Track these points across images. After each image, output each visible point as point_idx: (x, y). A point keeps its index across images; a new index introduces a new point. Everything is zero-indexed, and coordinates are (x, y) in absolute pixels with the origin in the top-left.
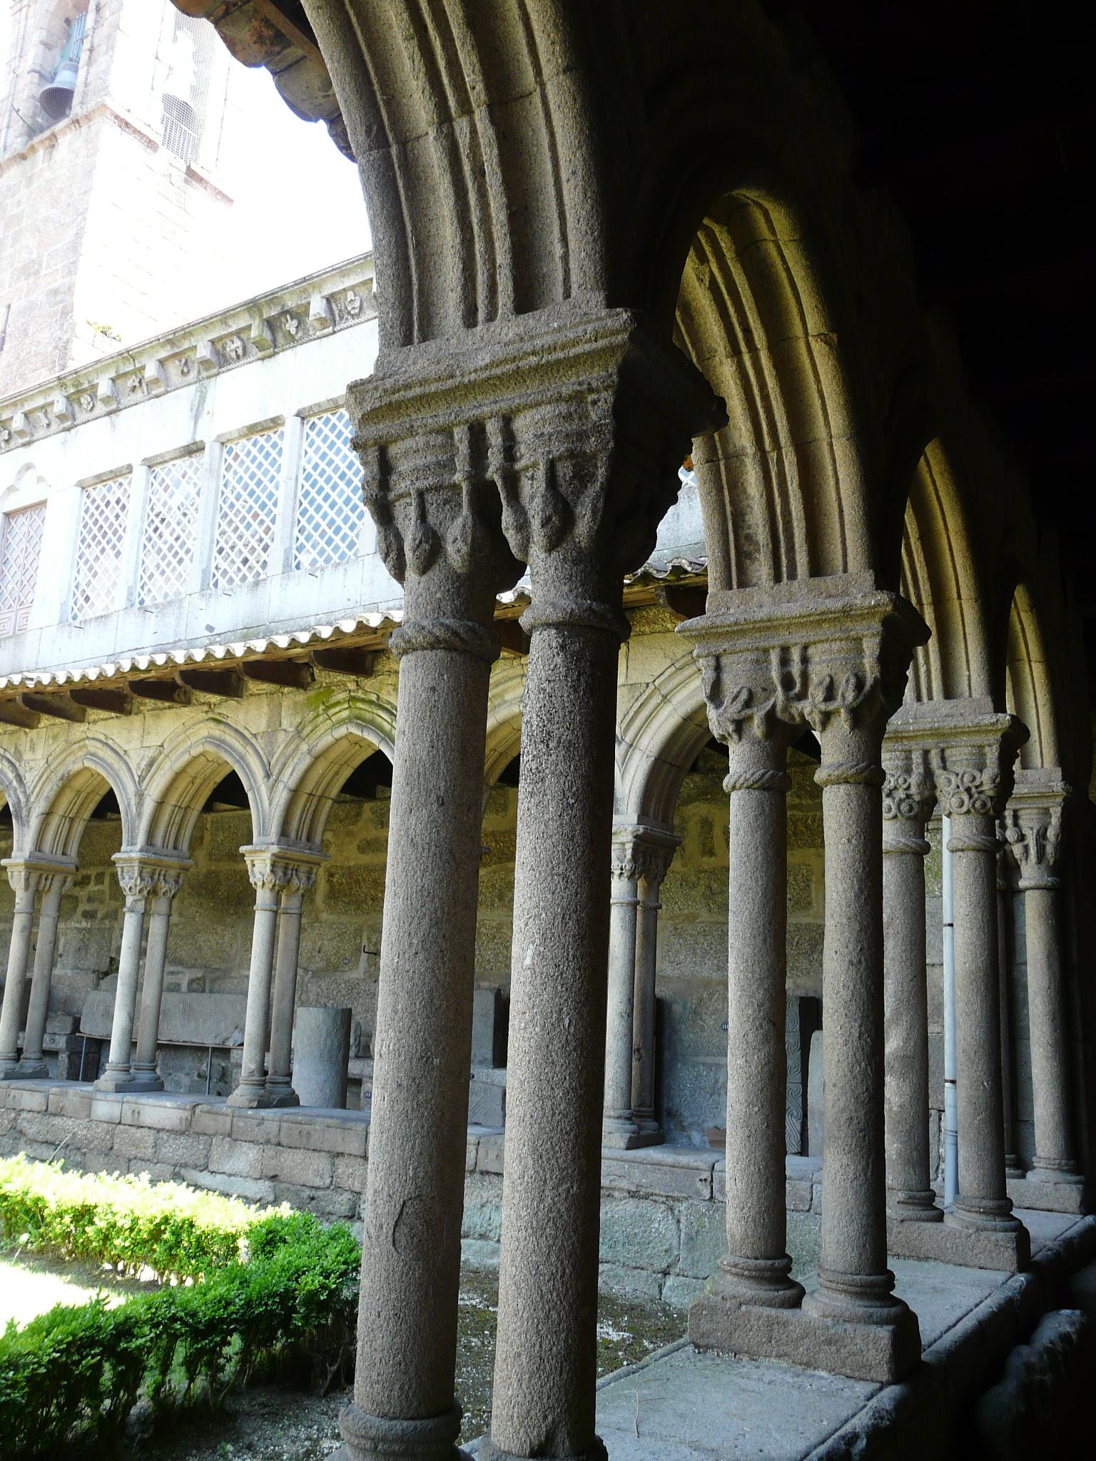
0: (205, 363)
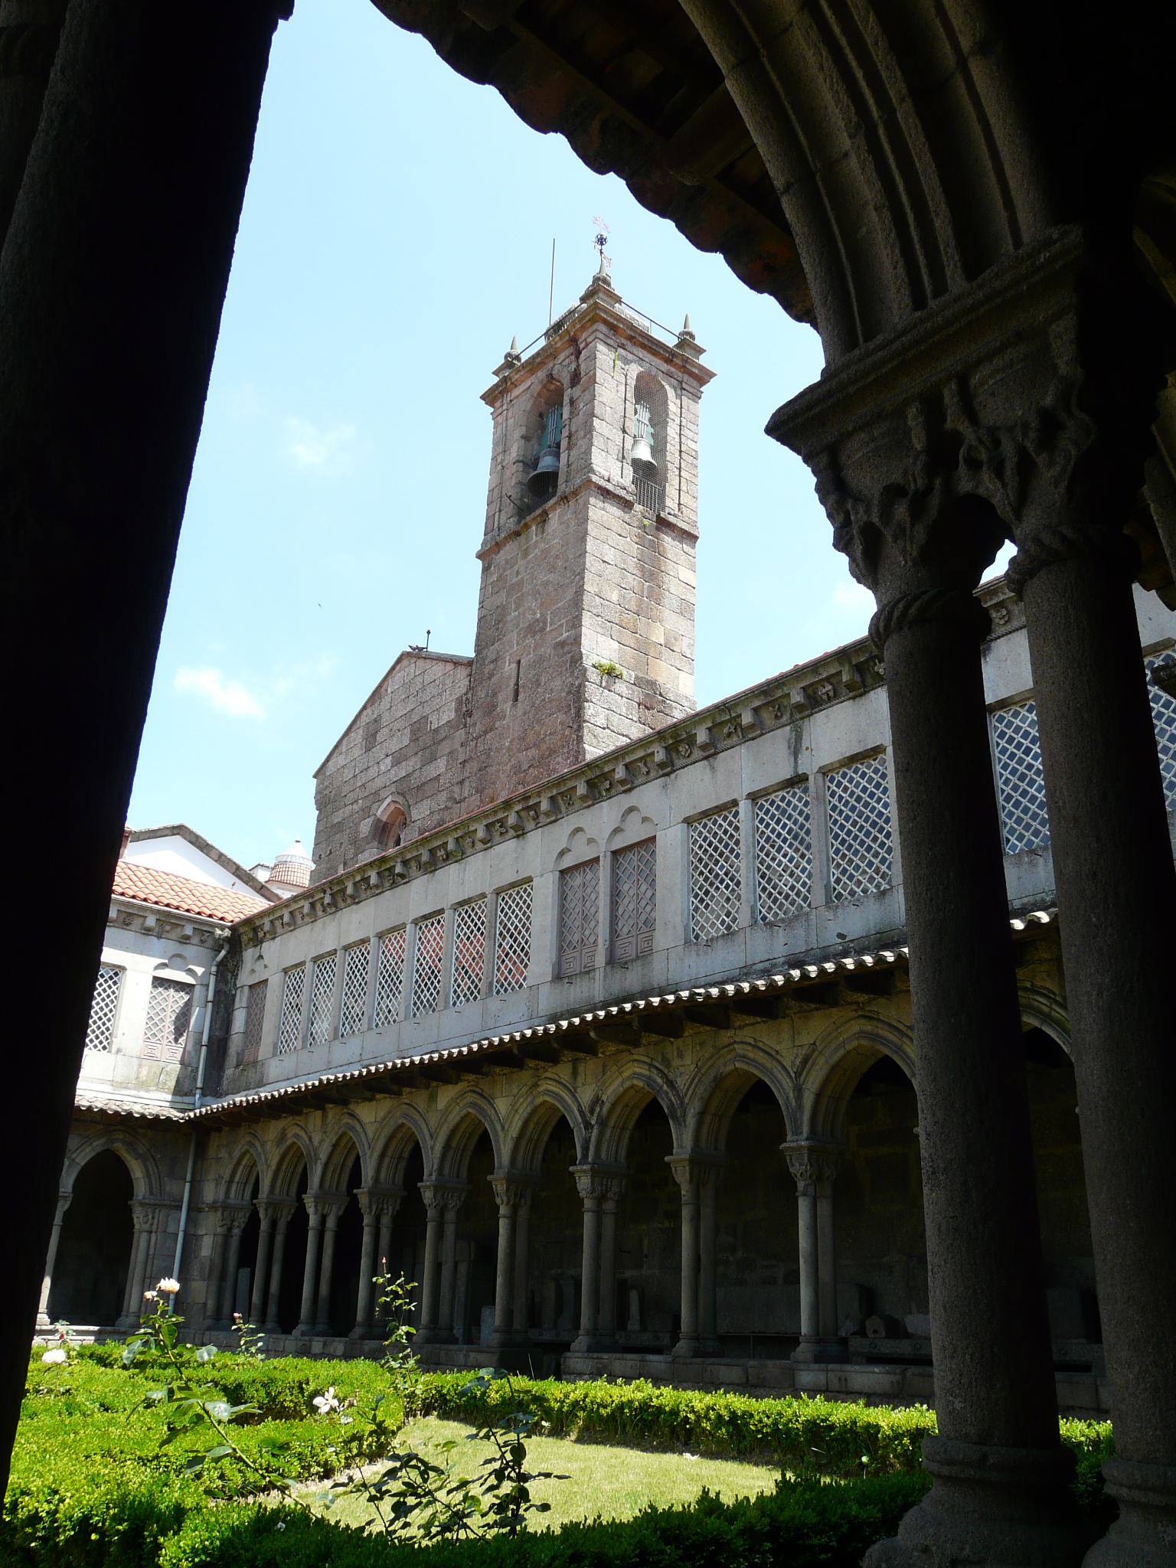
0: (799, 707)
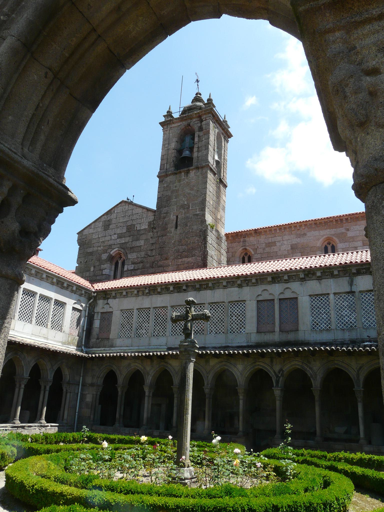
0: (354, 274)
